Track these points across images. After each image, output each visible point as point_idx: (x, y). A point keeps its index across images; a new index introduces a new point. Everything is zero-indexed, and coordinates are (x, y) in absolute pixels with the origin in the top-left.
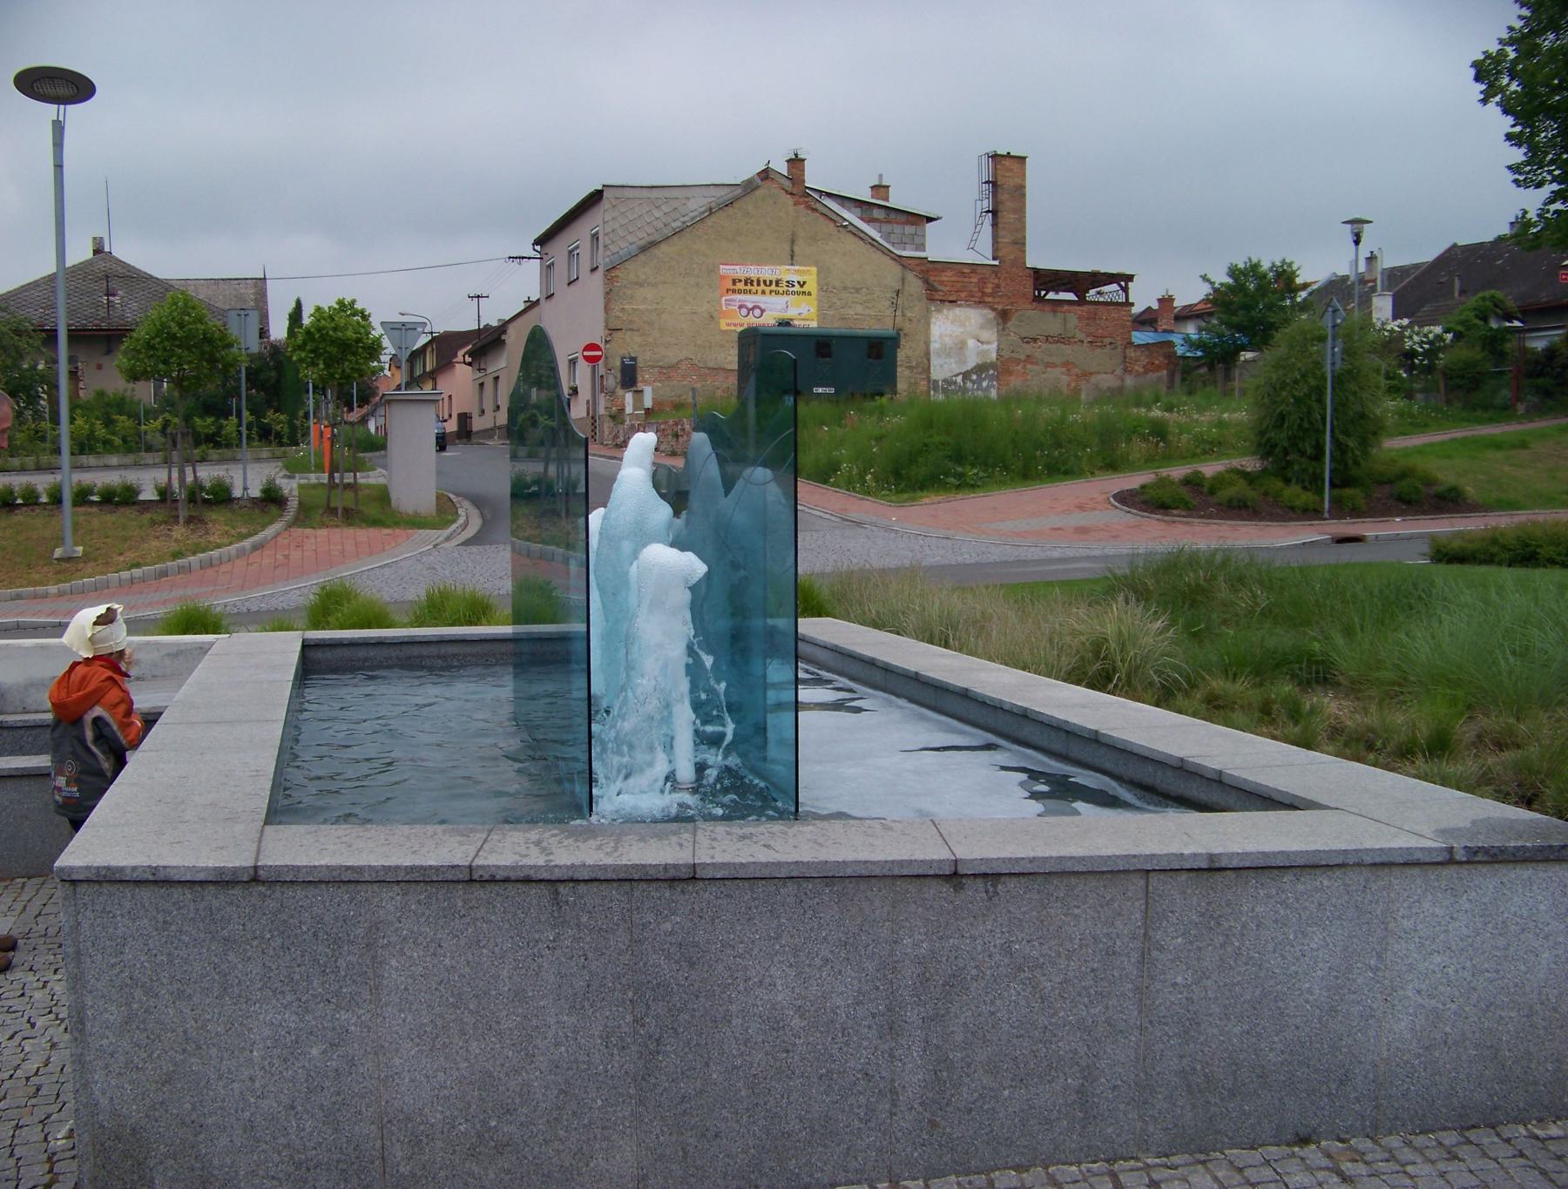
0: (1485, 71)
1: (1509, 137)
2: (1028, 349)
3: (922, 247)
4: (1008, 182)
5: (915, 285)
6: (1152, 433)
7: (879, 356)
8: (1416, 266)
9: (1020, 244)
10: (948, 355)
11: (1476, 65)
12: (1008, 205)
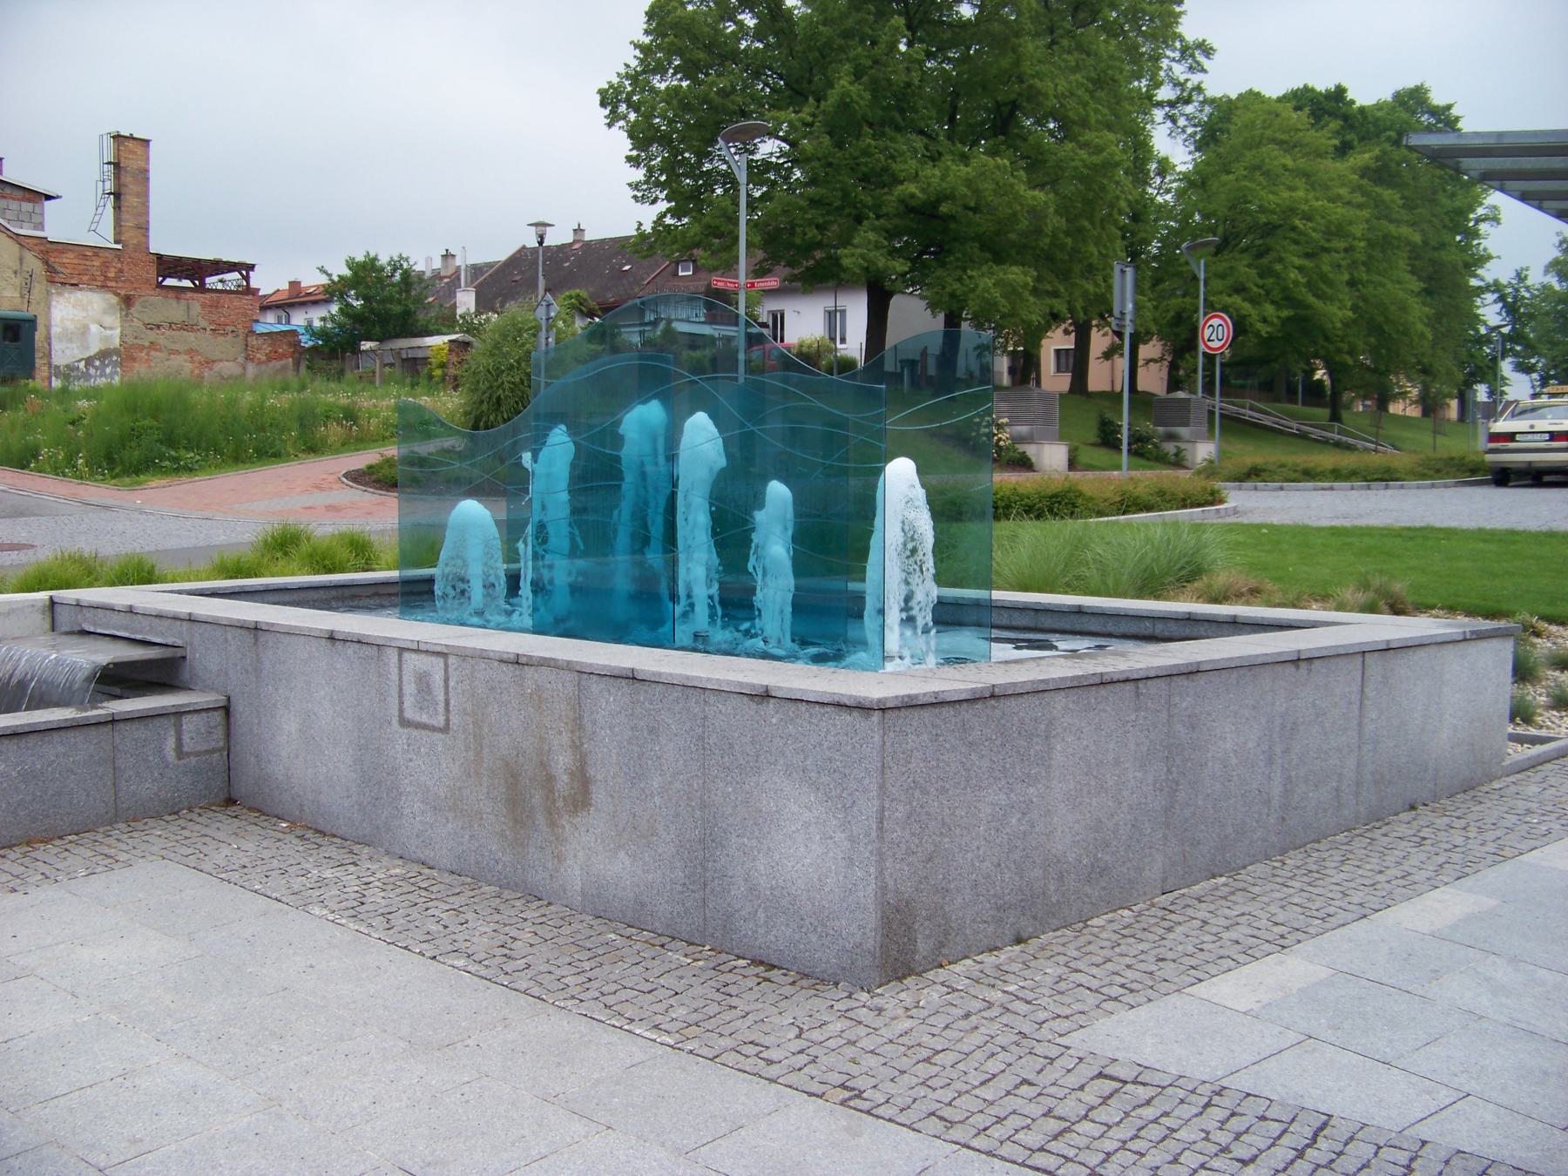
0: (609, 98)
1: (629, 159)
2: (152, 335)
3: (41, 226)
4: (131, 163)
5: (33, 263)
6: (345, 418)
7: (16, 338)
8: (490, 265)
9: (144, 229)
10: (70, 340)
11: (602, 92)
12: (131, 187)
